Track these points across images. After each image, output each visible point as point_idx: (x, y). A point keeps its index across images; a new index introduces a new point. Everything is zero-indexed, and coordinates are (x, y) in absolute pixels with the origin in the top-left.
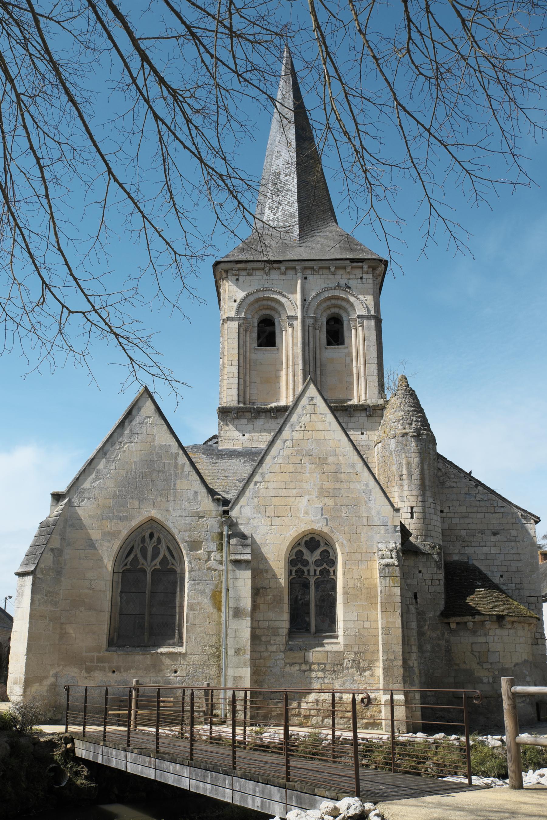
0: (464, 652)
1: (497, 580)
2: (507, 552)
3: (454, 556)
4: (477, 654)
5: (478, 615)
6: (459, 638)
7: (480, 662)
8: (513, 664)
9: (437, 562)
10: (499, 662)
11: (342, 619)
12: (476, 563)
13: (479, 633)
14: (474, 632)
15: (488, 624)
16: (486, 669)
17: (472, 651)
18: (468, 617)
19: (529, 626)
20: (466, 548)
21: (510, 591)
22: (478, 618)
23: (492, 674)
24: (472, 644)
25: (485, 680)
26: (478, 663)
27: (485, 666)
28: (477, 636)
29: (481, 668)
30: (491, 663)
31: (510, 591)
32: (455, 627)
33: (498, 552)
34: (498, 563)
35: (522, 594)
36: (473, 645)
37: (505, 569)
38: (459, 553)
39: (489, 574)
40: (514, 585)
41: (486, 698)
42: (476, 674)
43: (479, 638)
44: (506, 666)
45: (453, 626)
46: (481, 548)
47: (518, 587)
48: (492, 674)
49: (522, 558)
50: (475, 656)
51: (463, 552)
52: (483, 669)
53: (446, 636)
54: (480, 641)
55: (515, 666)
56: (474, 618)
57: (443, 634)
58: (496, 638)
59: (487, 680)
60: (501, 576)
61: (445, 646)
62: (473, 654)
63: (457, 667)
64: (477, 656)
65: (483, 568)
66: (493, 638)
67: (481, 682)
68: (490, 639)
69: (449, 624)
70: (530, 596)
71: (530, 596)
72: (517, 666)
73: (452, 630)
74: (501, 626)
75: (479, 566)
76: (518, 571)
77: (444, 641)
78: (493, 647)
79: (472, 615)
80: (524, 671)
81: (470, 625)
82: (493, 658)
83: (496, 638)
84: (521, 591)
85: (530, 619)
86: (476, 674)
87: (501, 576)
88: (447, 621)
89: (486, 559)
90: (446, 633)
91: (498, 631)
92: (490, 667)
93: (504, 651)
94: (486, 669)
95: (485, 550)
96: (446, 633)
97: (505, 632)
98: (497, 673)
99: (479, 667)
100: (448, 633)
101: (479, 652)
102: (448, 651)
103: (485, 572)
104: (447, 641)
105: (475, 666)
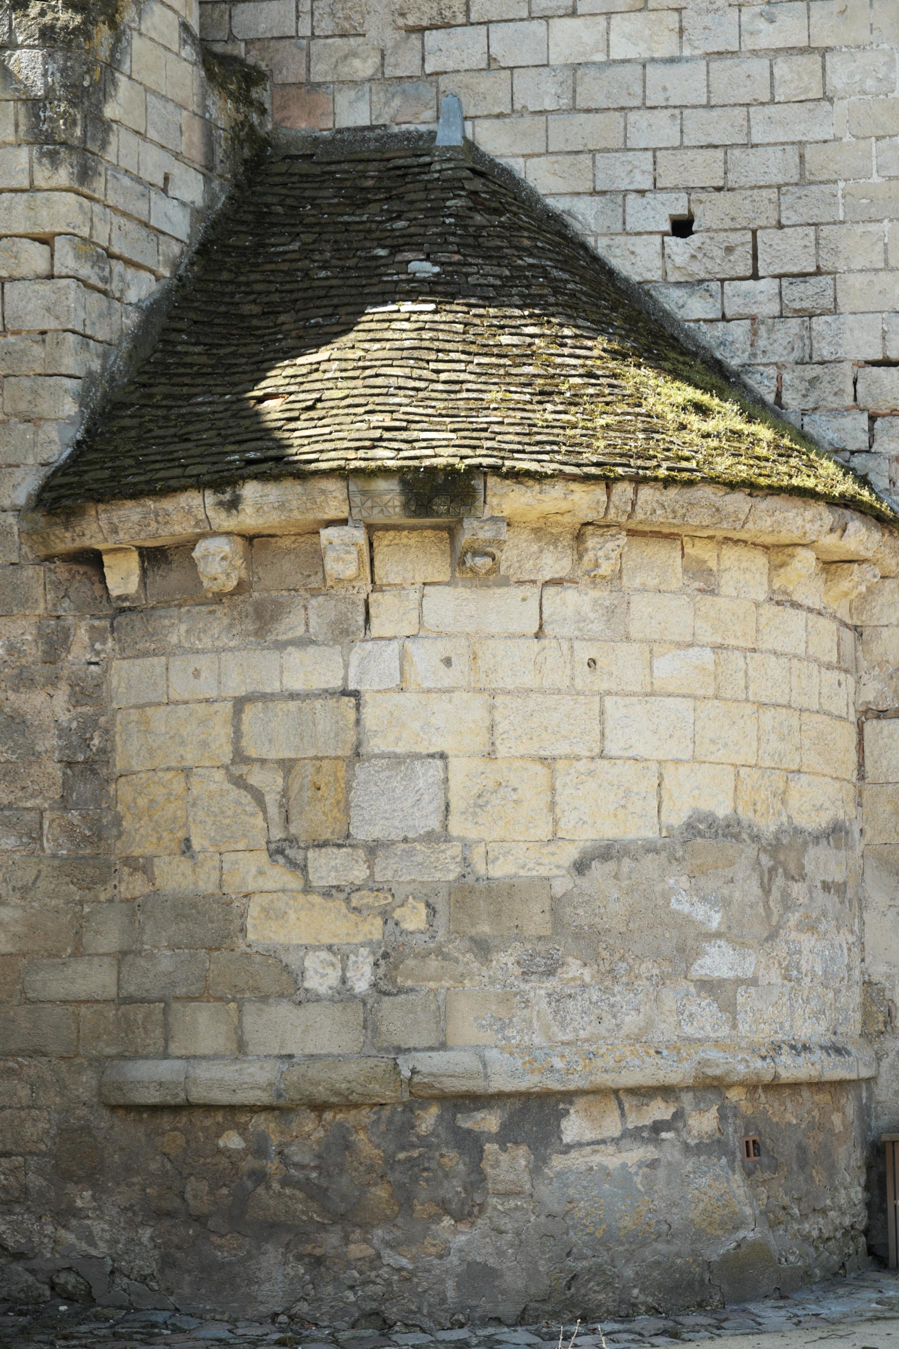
0: (187, 772)
1: (638, 256)
2: (726, 40)
3: (343, 99)
4: (269, 781)
5: (263, 477)
6: (158, 662)
7: (291, 840)
8: (570, 853)
9: (34, 105)
10: (439, 837)
11: (334, 654)
12: (496, 142)
13: (292, 625)
14: (256, 612)
15: (342, 551)
16: (327, 893)
17: (240, 757)
18: (192, 500)
19: (776, 567)
20: (432, 37)
21: (739, 331)
22: (261, 503)
23: (374, 929)
24: (240, 703)
25: (320, 977)
26: (276, 852)
27: (326, 867)
28: (281, 646)
29: (293, 882)
30: (373, 849)
31: (739, 331)
32: (132, 586)
33: (667, 47)
34: (658, 130)
35: (825, 351)
36: (250, 712)
37: (705, 169)
38: (381, 78)
39: (587, 218)
40: (767, 286)
41: (319, 1107)
42: (261, 932)
43: (294, 656)
44: (498, 871)
45: (123, 577)
46: (538, 27)
47: (800, 295)
48: (374, 929)
49: (837, 80)
50: (258, 797)
51: (406, 63)
52: (307, 889)
53: (79, 651)
54: (296, 684)
55: (581, 867)
56: (233, 505)
57: (55, 644)
58: (425, 658)
59: (333, 977)
60: (682, 227)
61: (63, 733)
62: (239, 782)
63: (137, 886)
64: (271, 799)
65: (545, 179)
66: (403, 656)
67: (289, 986)
68: (371, 667)
69: (92, 560)
70: (886, 363)
71: (886, 363)
72: (598, 869)
73: (122, 609)
74: (471, 565)
75: (518, 166)
76: (803, 182)
77: (62, 694)
78: (391, 723)
79: (217, 486)
80: (682, 905)
81: (218, 562)
82: (386, 809)
83: (425, 658)
84: (818, 323)
85: (738, 501)
86: (261, 932)
87: (682, 227)
88: (66, 541)
89: (574, 109)
90: (82, 634)
91: (450, 605)
92: (359, 873)
93: (491, 755)
94: (327, 893)
95: (570, 39)
96: (82, 634)
97: (511, 609)
98: (414, 919)
99: (280, 877)
100: (96, 635)
101: (287, 766)
102: (88, 764)
103: (557, 205)
104: (87, 692)
105: (253, 872)
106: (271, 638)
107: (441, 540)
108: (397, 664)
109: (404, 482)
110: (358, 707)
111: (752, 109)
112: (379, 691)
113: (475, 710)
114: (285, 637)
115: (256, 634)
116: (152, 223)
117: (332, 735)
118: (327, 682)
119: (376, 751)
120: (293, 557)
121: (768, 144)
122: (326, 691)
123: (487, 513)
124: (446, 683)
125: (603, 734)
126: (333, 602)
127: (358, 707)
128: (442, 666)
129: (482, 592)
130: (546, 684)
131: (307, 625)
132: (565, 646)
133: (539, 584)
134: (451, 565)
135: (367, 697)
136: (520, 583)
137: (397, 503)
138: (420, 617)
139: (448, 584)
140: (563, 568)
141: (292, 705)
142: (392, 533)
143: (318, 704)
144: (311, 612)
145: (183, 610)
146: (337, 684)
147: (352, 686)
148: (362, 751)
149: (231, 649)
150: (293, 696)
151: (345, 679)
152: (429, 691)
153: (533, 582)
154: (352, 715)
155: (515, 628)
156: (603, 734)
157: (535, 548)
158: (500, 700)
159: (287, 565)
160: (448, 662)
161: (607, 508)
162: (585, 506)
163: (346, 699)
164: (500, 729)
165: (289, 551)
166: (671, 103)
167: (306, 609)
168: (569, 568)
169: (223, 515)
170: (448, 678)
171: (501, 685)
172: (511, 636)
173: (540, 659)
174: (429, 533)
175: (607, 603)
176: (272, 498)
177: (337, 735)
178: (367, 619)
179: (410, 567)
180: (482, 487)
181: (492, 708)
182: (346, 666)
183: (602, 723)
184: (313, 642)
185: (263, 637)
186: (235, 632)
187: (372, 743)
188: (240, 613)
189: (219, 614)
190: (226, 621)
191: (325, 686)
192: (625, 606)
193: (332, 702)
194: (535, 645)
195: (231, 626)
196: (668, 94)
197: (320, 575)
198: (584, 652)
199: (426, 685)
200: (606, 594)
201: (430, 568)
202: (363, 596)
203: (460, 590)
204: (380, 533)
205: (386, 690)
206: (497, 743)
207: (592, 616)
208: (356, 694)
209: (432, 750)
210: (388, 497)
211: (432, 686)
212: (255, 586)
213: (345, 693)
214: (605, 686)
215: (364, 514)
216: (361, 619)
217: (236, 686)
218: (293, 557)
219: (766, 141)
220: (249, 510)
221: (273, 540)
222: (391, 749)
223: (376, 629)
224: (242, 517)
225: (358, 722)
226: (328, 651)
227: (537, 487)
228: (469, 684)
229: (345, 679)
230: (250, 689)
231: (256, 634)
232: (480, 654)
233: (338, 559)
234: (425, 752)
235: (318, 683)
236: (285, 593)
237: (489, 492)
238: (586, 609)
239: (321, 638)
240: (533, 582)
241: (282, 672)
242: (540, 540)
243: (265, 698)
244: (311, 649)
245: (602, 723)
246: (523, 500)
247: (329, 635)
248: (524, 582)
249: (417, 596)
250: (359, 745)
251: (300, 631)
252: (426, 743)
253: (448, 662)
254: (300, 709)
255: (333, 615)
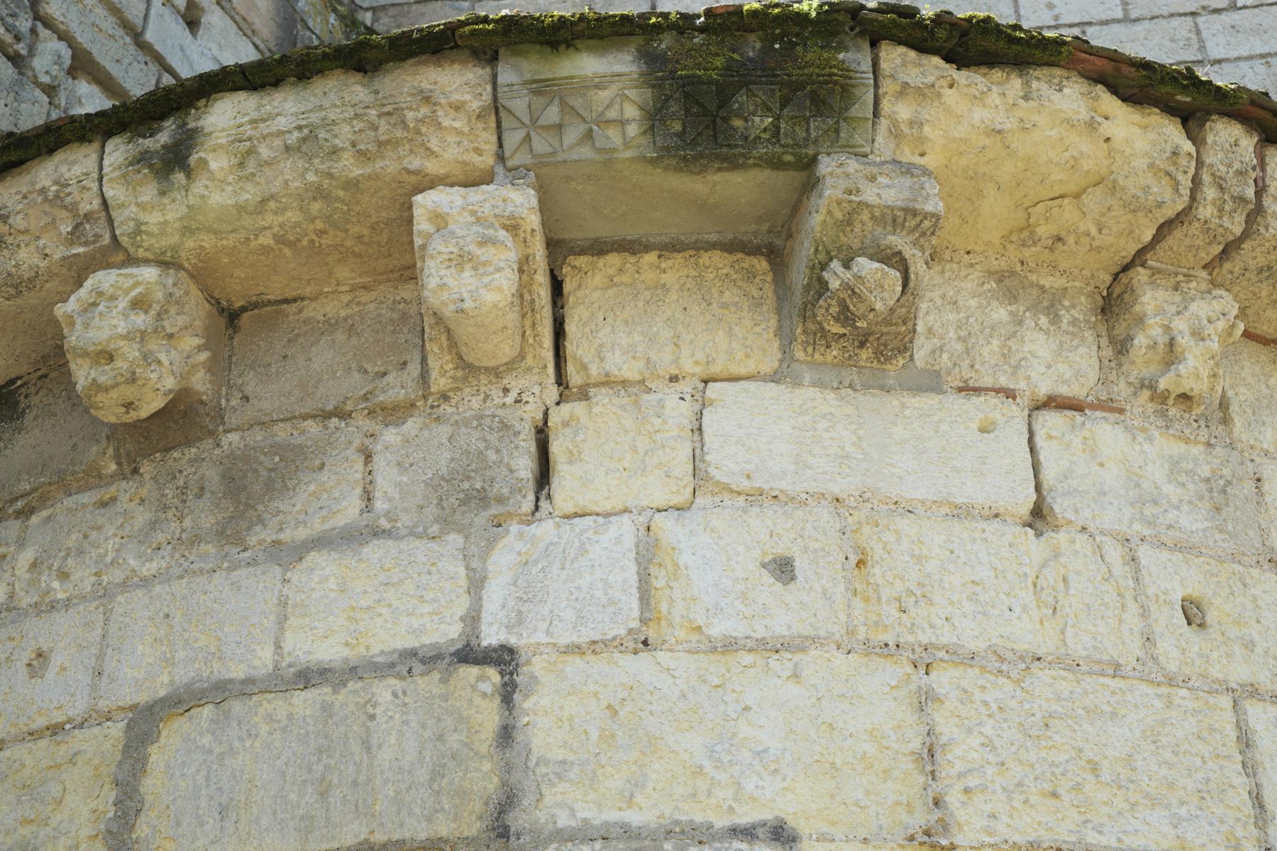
11: (447, 559)
13: (330, 497)
24: (144, 723)
28: (288, 555)
43: (324, 569)
66: (648, 554)
74: (839, 324)
91: (781, 425)
106: (260, 536)
107: (750, 275)
108: (631, 574)
109: (650, 58)
110: (508, 694)
111: (1200, 20)
112: (575, 649)
113: (875, 703)
114: (302, 533)
115: (221, 533)
116: (149, 36)
117: (423, 774)
118: (414, 632)
119: (564, 821)
120: (340, 336)
121: (1238, 59)
122: (413, 653)
123: (883, 145)
124: (781, 624)
125: (1258, 800)
126: (444, 430)
127: (508, 694)
128: (768, 579)
129: (867, 400)
130: (1079, 646)
131: (368, 497)
132: (1114, 554)
133: (1025, 401)
134: (779, 332)
135: (536, 667)
136: (967, 389)
137: (631, 112)
138: (696, 458)
139: (774, 378)
140: (1078, 374)
141: (304, 702)
142: (614, 259)
143: (383, 691)
144: (379, 463)
145: (34, 520)
146: (449, 632)
147: (491, 636)
148: (517, 820)
149: (146, 582)
150: (307, 677)
151: (473, 619)
152: (729, 646)
153: (1010, 394)
154: (489, 716)
155: (968, 492)
156: (1258, 800)
157: (1001, 313)
158: (944, 679)
159: (323, 356)
160: (783, 569)
161: (1196, 182)
162: (1140, 163)
163: (473, 671)
164: (955, 759)
165: (331, 325)
166: (1061, 21)
167: (368, 457)
168: (1092, 375)
169: (148, 192)
170: (782, 612)
171: (947, 638)
172: (961, 512)
173: (1050, 577)
174: (716, 259)
175: (1205, 471)
176: (282, 123)
177: (437, 774)
178: (544, 476)
179: (667, 334)
180: (866, 65)
181: (925, 700)
182: (476, 584)
183: (1249, 768)
184: (378, 533)
185: (239, 540)
186: (161, 537)
187: (551, 797)
188: (183, 491)
189: (124, 503)
190: (142, 517)
191: (409, 643)
192: (1249, 486)
193: (428, 684)
194: (1032, 547)
195: (153, 525)
196: (1056, 11)
197: (414, 369)
198: (1171, 578)
199: (717, 629)
200: (1197, 450)
201: (721, 337)
202: (532, 412)
203: (808, 394)
204: (582, 261)
205: (595, 647)
206: (953, 799)
207: (1169, 490)
208: (504, 658)
209: (745, 817)
210: (605, 95)
211: (738, 629)
212: (232, 420)
213: (469, 655)
214: (1240, 673)
215: (540, 145)
216: (525, 466)
217: (140, 674)
218: (340, 336)
219: (1235, 54)
220: (218, 163)
221: (292, 308)
222: (613, 816)
223: (568, 486)
224: (198, 188)
225: (506, 735)
226: (421, 549)
227: (1016, 83)
228: (851, 632)
229: (473, 619)
230: (182, 675)
231: (221, 533)
232: (877, 551)
233: (461, 260)
234: (721, 822)
235: (389, 635)
236: (313, 427)
237: (888, 87)
238: (1156, 473)
239: (405, 521)
240: (1010, 394)
241: (282, 620)
242: (1012, 297)
243: (221, 692)
244: (374, 551)
245: (1249, 768)
246: (979, 115)
247: (431, 511)
248: (977, 390)
249: (687, 408)
250: (508, 801)
251: (349, 511)
252: (724, 794)
253: (783, 569)
254: (327, 709)
255: (443, 460)
